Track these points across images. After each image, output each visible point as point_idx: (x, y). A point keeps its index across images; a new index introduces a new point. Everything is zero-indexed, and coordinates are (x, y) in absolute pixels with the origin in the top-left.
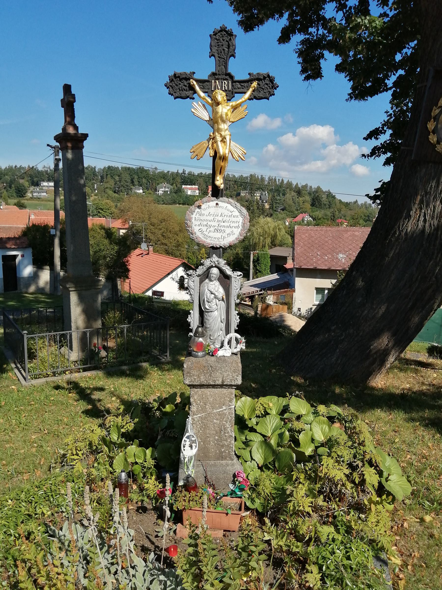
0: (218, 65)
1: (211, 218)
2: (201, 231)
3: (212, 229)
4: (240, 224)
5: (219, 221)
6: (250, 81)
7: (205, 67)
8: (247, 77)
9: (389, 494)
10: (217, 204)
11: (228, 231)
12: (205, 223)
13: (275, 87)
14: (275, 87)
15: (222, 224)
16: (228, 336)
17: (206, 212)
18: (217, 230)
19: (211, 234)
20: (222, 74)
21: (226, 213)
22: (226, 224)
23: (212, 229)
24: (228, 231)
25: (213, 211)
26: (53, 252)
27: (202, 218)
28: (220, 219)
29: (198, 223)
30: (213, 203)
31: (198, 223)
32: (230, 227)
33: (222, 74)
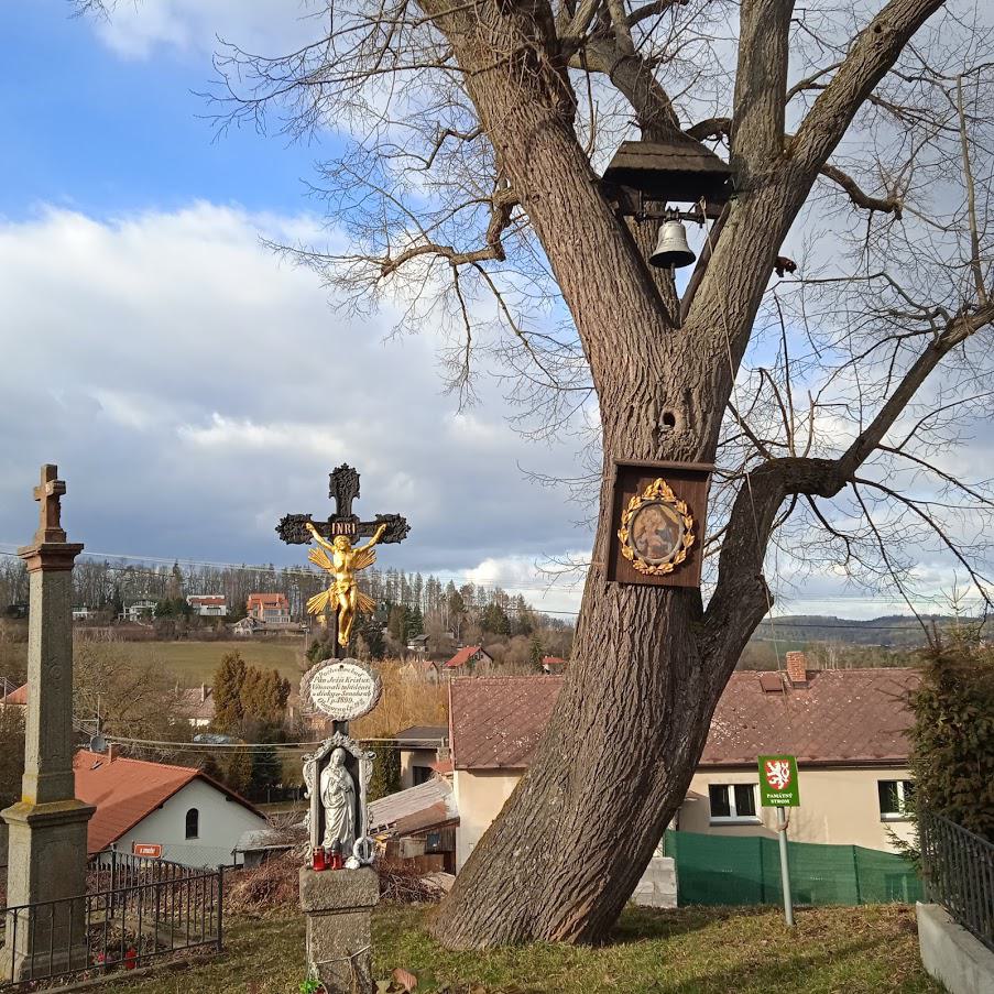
0: (339, 507)
1: (332, 684)
2: (323, 702)
3: (336, 698)
4: (372, 690)
5: (344, 687)
6: (378, 523)
7: (325, 508)
8: (375, 519)
9: (412, 974)
10: (342, 667)
11: (356, 699)
12: (327, 691)
13: (345, 467)
14: (345, 467)
15: (349, 691)
16: (359, 841)
17: (328, 678)
18: (341, 700)
19: (334, 705)
20: (343, 514)
21: (353, 677)
22: (353, 691)
23: (336, 698)
24: (356, 699)
25: (336, 675)
26: (25, 661)
27: (323, 685)
28: (346, 684)
29: (318, 691)
30: (337, 666)
31: (318, 691)
32: (358, 694)
33: (343, 514)
